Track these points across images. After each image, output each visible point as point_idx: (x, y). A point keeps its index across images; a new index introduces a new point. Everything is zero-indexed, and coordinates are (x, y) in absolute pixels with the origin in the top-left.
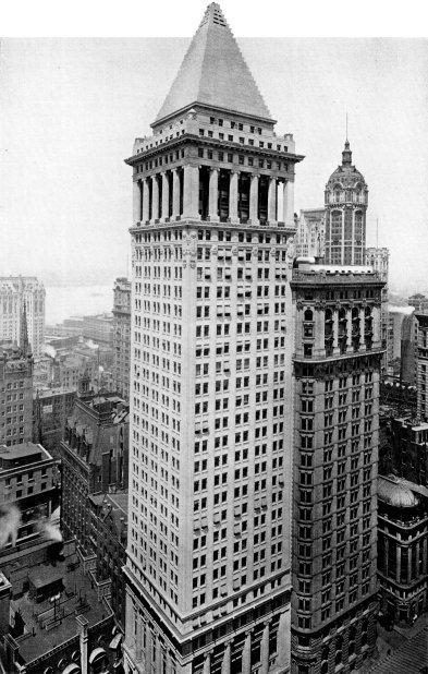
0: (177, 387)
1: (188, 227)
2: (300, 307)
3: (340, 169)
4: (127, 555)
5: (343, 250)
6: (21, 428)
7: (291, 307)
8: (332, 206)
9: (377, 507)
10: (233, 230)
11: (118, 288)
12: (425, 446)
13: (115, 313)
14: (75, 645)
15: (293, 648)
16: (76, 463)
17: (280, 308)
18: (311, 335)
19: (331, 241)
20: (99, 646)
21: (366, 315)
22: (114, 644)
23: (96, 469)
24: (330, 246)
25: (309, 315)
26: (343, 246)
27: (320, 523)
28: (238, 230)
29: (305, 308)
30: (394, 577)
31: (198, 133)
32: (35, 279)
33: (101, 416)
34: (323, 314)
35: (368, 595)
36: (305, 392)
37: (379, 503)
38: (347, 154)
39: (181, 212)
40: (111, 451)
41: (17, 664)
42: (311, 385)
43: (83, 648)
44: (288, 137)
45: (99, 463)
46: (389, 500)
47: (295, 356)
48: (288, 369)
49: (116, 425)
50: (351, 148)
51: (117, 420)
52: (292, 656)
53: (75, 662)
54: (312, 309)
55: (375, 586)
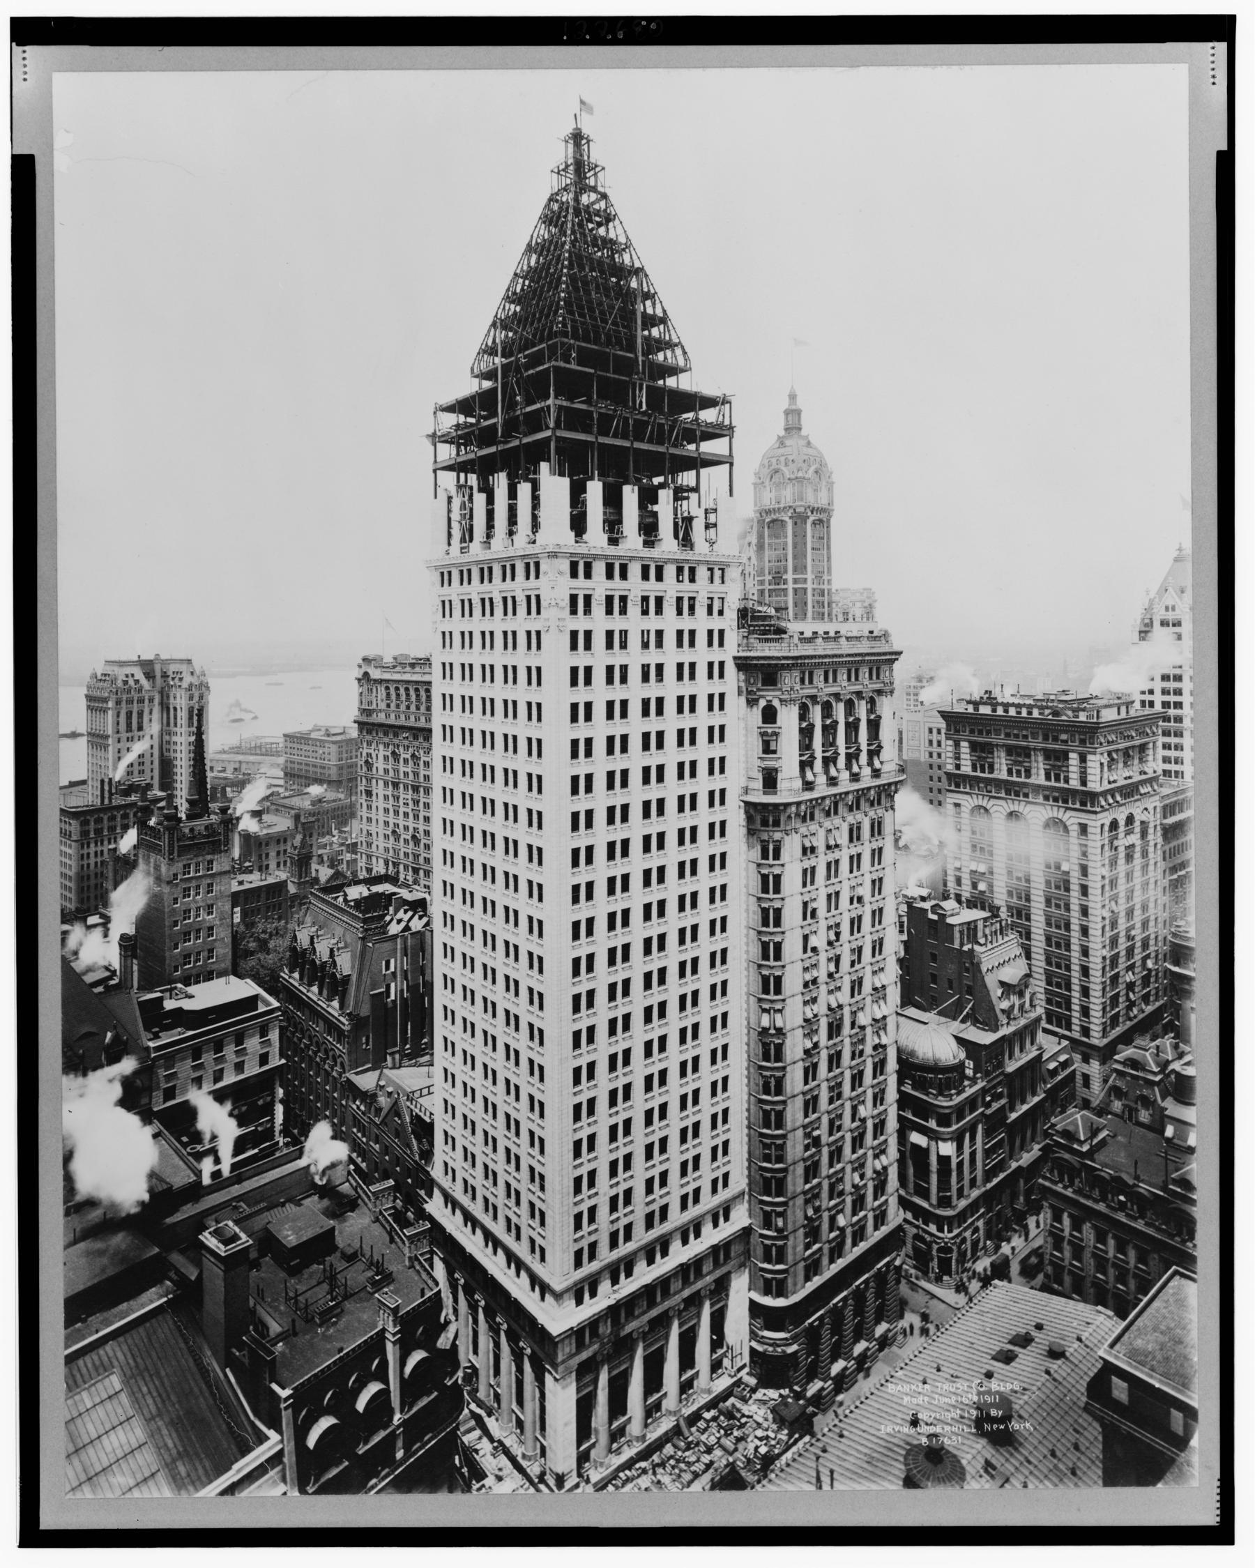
0: (536, 855)
1: (553, 555)
2: (751, 703)
3: (781, 442)
5: (790, 592)
6: (211, 951)
7: (736, 704)
8: (768, 512)
9: (896, 1067)
10: (699, 562)
11: (366, 674)
12: (972, 951)
13: (362, 725)
14: (376, 1345)
15: (753, 1335)
16: (316, 1014)
17: (717, 702)
18: (774, 752)
19: (768, 578)
20: (419, 1346)
21: (824, 717)
22: (443, 1342)
24: (767, 587)
25: (769, 715)
26: (790, 586)
27: (799, 1101)
28: (606, 557)
29: (763, 703)
30: (925, 1194)
32: (189, 661)
33: (365, 921)
34: (795, 711)
35: (884, 1230)
37: (900, 1060)
39: (535, 526)
40: (388, 987)
41: (275, 1387)
43: (391, 1352)
47: (746, 791)
49: (395, 937)
50: (800, 403)
51: (394, 929)
53: (376, 1379)
54: (776, 703)
55: (896, 1216)
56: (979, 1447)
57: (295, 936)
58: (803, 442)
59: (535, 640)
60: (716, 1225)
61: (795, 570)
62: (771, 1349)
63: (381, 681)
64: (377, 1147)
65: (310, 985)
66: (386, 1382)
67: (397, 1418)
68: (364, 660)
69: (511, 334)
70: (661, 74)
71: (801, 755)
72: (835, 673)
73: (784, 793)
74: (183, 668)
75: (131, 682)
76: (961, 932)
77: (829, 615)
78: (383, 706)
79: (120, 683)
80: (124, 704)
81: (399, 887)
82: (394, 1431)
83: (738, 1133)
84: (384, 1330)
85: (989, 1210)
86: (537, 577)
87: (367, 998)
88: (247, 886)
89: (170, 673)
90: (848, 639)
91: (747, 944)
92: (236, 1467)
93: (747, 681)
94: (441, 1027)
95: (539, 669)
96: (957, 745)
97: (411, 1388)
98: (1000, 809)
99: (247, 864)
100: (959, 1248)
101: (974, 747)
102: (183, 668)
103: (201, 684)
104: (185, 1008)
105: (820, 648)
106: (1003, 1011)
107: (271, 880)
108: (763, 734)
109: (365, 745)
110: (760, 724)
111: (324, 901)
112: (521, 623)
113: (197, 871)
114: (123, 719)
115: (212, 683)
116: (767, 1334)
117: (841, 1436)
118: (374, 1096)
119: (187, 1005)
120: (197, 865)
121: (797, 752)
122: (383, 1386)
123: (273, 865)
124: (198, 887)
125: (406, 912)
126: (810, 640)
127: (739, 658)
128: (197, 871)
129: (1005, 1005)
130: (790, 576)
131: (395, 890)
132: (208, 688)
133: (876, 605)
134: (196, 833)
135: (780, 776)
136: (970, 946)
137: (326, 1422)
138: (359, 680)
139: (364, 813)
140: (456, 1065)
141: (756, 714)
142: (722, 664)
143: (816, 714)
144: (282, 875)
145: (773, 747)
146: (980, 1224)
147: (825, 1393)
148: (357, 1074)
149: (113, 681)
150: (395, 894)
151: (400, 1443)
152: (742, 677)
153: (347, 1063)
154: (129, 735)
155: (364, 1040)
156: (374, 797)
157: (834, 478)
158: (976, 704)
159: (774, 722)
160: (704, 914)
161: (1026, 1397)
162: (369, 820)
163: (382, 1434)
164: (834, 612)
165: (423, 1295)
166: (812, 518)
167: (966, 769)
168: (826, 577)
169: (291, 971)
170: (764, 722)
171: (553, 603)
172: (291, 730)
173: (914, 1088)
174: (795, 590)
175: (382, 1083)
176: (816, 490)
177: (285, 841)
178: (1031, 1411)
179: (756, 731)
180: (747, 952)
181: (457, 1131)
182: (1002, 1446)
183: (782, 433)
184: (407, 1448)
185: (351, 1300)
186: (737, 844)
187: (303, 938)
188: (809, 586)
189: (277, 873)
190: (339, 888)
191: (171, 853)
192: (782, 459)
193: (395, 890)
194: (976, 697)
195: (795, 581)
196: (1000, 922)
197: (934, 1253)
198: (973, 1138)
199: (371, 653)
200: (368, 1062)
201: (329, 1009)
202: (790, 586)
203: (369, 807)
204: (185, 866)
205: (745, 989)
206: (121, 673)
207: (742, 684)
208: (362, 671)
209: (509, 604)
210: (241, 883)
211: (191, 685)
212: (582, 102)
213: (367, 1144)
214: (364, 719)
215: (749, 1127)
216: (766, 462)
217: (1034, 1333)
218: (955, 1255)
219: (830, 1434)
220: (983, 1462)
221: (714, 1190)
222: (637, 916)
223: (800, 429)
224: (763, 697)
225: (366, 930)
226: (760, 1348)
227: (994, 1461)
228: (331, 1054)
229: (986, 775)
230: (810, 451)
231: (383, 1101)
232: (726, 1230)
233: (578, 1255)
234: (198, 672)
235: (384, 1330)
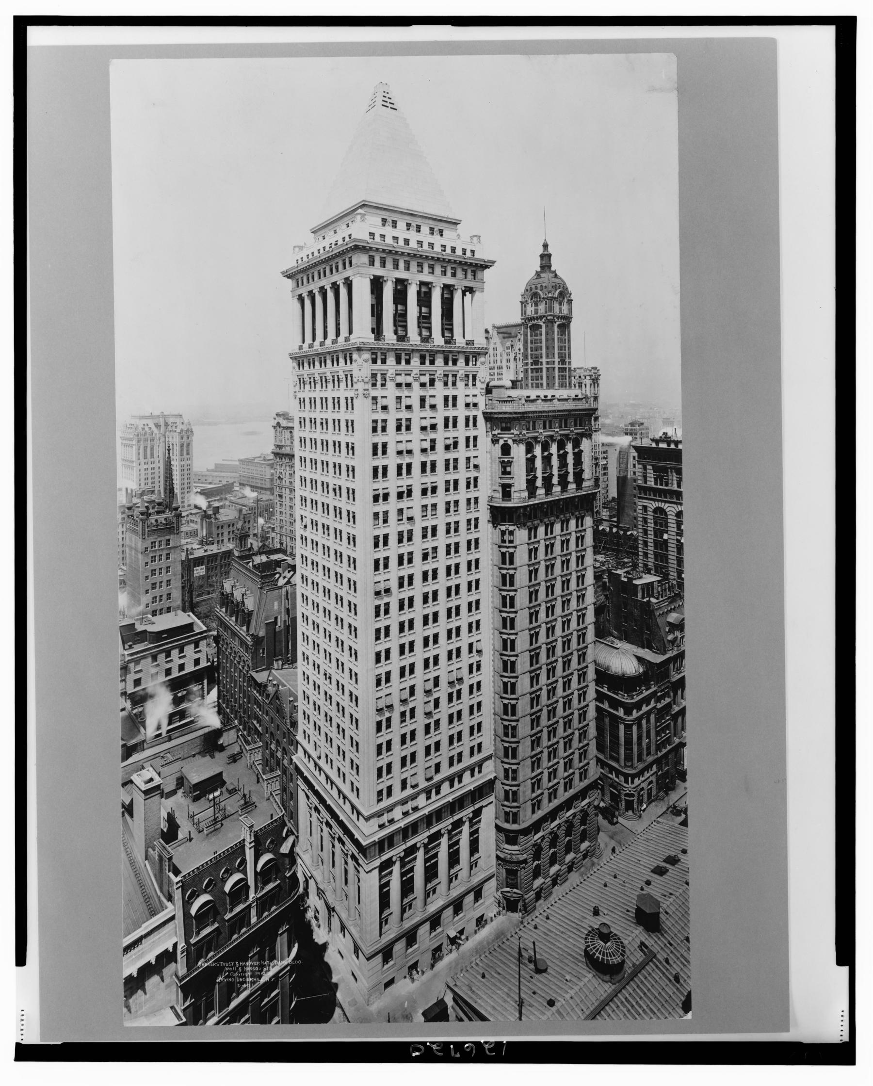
1: (359, 349)
2: (495, 441)
3: (538, 274)
5: (544, 370)
7: (484, 441)
8: (530, 319)
9: (595, 677)
11: (278, 424)
13: (276, 454)
15: (498, 848)
16: (234, 634)
18: (509, 473)
19: (530, 361)
21: (543, 451)
22: (285, 849)
24: (530, 367)
25: (506, 450)
26: (544, 366)
29: (501, 442)
32: (181, 416)
33: (262, 577)
34: (522, 448)
37: (597, 671)
38: (546, 257)
43: (249, 854)
44: (475, 239)
45: (262, 633)
47: (491, 498)
48: (483, 514)
49: (281, 587)
50: (550, 250)
51: (281, 582)
53: (239, 871)
54: (510, 442)
55: (594, 771)
56: (637, 932)
57: (223, 586)
58: (552, 275)
59: (350, 402)
60: (472, 775)
61: (547, 356)
62: (509, 856)
63: (287, 428)
64: (267, 718)
65: (231, 616)
66: (245, 874)
67: (252, 895)
68: (277, 415)
71: (527, 476)
72: (550, 422)
73: (516, 501)
74: (178, 420)
75: (147, 429)
76: (643, 590)
77: (570, 384)
78: (288, 443)
79: (140, 430)
80: (142, 442)
81: (287, 556)
82: (250, 905)
83: (488, 718)
84: (244, 840)
85: (659, 769)
86: (351, 363)
87: (263, 625)
88: (209, 553)
89: (170, 423)
90: (559, 400)
91: (493, 597)
92: (144, 925)
94: (301, 646)
95: (352, 421)
96: (645, 468)
97: (263, 877)
98: (672, 509)
99: (210, 539)
100: (639, 794)
101: (655, 469)
102: (178, 420)
103: (188, 430)
104: (149, 630)
105: (540, 406)
106: (669, 641)
107: (224, 549)
108: (502, 462)
109: (278, 467)
110: (500, 456)
111: (241, 565)
112: (342, 393)
113: (160, 546)
114: (142, 451)
115: (194, 429)
116: (507, 846)
117: (548, 918)
118: (266, 686)
119: (151, 628)
120: (160, 542)
121: (524, 474)
122: (242, 876)
123: (226, 540)
124: (161, 556)
125: (289, 572)
126: (534, 401)
127: (487, 413)
128: (160, 546)
129: (670, 637)
130: (544, 360)
131: (285, 558)
132: (192, 432)
133: (600, 378)
134: (159, 522)
135: (513, 489)
136: (648, 599)
137: (205, 898)
138: (274, 427)
139: (278, 508)
140: (310, 671)
141: (498, 448)
142: (475, 418)
143: (538, 450)
144: (230, 546)
145: (508, 469)
146: (653, 778)
147: (545, 886)
148: (257, 672)
149: (136, 428)
150: (285, 560)
151: (253, 912)
152: (489, 426)
153: (251, 665)
154: (146, 460)
155: (261, 651)
156: (284, 500)
157: (572, 297)
158: (657, 442)
159: (509, 454)
160: (463, 578)
161: (671, 900)
162: (281, 513)
163: (241, 907)
164: (573, 382)
165: (272, 819)
166: (558, 323)
167: (651, 483)
168: (567, 360)
169: (221, 607)
170: (503, 454)
171: (360, 379)
172: (243, 457)
173: (609, 690)
174: (548, 369)
175: (270, 678)
176: (560, 304)
177: (233, 525)
178: (674, 909)
179: (498, 460)
180: (493, 602)
181: (310, 711)
182: (653, 932)
183: (539, 269)
184: (259, 915)
185: (228, 820)
186: (487, 533)
187: (227, 586)
188: (557, 366)
189: (228, 545)
190: (249, 557)
191: (143, 534)
192: (539, 286)
193: (285, 558)
194: (657, 437)
195: (548, 363)
196: (668, 583)
197: (623, 797)
198: (648, 721)
199: (280, 410)
200: (264, 665)
201: (241, 632)
202: (544, 366)
203: (281, 505)
204: (152, 543)
205: (491, 626)
206: (140, 423)
208: (276, 422)
209: (335, 380)
210: (206, 551)
211: (182, 430)
213: (262, 716)
214: (278, 451)
215: (495, 714)
216: (528, 288)
217: (681, 856)
218: (635, 798)
219: (540, 916)
220: (639, 943)
221: (451, 764)
222: (418, 579)
223: (550, 266)
224: (502, 438)
225: (263, 583)
226: (502, 856)
227: (647, 943)
228: (242, 658)
229: (664, 487)
230: (556, 280)
231: (271, 690)
232: (480, 779)
233: (380, 793)
234: (186, 422)
235: (244, 840)
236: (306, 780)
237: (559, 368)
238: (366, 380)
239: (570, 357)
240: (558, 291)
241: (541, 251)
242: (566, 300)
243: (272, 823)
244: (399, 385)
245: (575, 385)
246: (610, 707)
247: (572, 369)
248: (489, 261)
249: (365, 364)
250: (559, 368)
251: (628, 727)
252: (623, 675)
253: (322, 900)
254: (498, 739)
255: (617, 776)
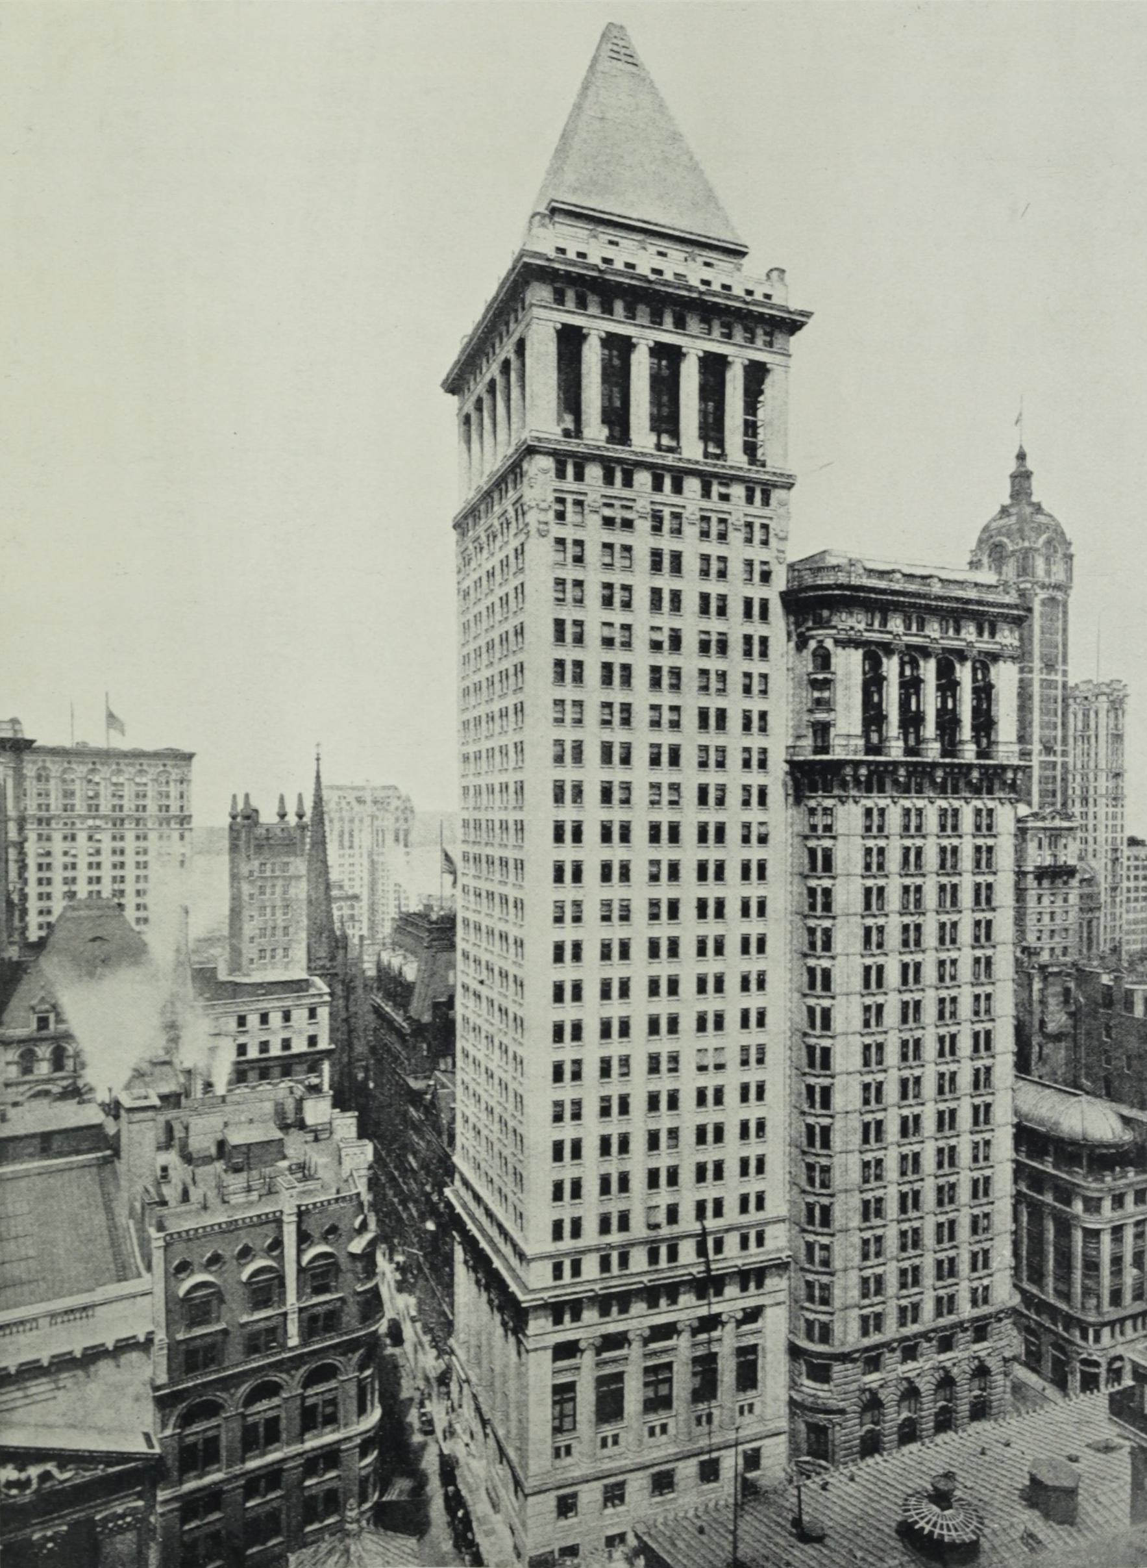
2: (801, 645)
3: (1004, 511)
4: (454, 1166)
15: (794, 1385)
23: (419, 1029)
25: (823, 660)
29: (813, 644)
31: (552, 254)
34: (857, 655)
36: (814, 828)
38: (1021, 479)
42: (827, 811)
44: (775, 274)
45: (426, 1018)
46: (1057, 1123)
48: (776, 778)
50: (1030, 464)
52: (792, 1402)
54: (829, 644)
69: (396, 1241)
70: (503, 274)
93: (798, 625)
100: (1110, 1363)
113: (273, 871)
135: (833, 731)
141: (806, 664)
152: (792, 619)
207: (792, 628)
212: (111, 716)
224: (812, 637)
226: (796, 1397)
236: (470, 1243)
237: (1042, 680)
238: (544, 505)
239: (1065, 662)
240: (1044, 537)
241: (1012, 466)
242: (1060, 555)
243: (337, 1200)
244: (608, 522)
245: (1075, 715)
246: (1056, 1199)
247: (1071, 684)
248: (803, 314)
249: (541, 477)
250: (1042, 680)
251: (1092, 1235)
252: (1084, 1134)
253: (491, 1442)
254: (796, 1190)
255: (1066, 1329)
